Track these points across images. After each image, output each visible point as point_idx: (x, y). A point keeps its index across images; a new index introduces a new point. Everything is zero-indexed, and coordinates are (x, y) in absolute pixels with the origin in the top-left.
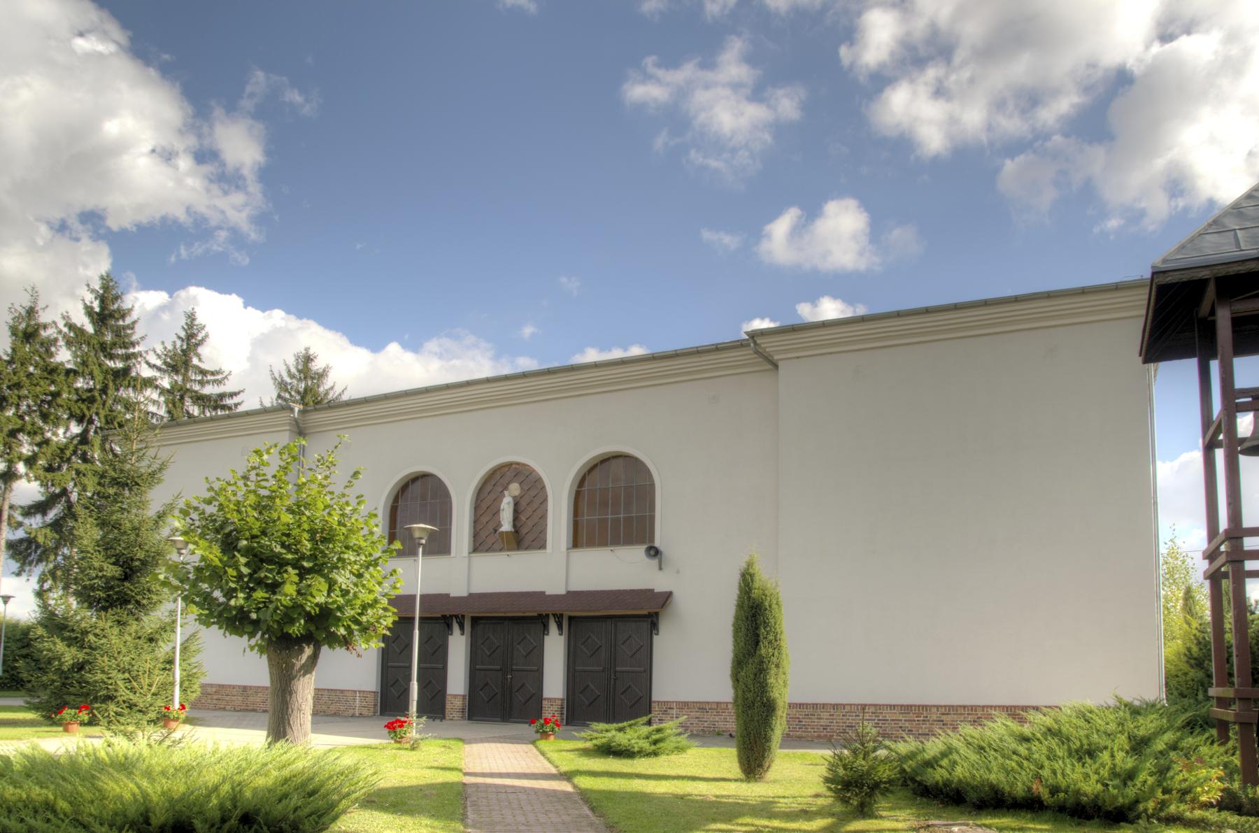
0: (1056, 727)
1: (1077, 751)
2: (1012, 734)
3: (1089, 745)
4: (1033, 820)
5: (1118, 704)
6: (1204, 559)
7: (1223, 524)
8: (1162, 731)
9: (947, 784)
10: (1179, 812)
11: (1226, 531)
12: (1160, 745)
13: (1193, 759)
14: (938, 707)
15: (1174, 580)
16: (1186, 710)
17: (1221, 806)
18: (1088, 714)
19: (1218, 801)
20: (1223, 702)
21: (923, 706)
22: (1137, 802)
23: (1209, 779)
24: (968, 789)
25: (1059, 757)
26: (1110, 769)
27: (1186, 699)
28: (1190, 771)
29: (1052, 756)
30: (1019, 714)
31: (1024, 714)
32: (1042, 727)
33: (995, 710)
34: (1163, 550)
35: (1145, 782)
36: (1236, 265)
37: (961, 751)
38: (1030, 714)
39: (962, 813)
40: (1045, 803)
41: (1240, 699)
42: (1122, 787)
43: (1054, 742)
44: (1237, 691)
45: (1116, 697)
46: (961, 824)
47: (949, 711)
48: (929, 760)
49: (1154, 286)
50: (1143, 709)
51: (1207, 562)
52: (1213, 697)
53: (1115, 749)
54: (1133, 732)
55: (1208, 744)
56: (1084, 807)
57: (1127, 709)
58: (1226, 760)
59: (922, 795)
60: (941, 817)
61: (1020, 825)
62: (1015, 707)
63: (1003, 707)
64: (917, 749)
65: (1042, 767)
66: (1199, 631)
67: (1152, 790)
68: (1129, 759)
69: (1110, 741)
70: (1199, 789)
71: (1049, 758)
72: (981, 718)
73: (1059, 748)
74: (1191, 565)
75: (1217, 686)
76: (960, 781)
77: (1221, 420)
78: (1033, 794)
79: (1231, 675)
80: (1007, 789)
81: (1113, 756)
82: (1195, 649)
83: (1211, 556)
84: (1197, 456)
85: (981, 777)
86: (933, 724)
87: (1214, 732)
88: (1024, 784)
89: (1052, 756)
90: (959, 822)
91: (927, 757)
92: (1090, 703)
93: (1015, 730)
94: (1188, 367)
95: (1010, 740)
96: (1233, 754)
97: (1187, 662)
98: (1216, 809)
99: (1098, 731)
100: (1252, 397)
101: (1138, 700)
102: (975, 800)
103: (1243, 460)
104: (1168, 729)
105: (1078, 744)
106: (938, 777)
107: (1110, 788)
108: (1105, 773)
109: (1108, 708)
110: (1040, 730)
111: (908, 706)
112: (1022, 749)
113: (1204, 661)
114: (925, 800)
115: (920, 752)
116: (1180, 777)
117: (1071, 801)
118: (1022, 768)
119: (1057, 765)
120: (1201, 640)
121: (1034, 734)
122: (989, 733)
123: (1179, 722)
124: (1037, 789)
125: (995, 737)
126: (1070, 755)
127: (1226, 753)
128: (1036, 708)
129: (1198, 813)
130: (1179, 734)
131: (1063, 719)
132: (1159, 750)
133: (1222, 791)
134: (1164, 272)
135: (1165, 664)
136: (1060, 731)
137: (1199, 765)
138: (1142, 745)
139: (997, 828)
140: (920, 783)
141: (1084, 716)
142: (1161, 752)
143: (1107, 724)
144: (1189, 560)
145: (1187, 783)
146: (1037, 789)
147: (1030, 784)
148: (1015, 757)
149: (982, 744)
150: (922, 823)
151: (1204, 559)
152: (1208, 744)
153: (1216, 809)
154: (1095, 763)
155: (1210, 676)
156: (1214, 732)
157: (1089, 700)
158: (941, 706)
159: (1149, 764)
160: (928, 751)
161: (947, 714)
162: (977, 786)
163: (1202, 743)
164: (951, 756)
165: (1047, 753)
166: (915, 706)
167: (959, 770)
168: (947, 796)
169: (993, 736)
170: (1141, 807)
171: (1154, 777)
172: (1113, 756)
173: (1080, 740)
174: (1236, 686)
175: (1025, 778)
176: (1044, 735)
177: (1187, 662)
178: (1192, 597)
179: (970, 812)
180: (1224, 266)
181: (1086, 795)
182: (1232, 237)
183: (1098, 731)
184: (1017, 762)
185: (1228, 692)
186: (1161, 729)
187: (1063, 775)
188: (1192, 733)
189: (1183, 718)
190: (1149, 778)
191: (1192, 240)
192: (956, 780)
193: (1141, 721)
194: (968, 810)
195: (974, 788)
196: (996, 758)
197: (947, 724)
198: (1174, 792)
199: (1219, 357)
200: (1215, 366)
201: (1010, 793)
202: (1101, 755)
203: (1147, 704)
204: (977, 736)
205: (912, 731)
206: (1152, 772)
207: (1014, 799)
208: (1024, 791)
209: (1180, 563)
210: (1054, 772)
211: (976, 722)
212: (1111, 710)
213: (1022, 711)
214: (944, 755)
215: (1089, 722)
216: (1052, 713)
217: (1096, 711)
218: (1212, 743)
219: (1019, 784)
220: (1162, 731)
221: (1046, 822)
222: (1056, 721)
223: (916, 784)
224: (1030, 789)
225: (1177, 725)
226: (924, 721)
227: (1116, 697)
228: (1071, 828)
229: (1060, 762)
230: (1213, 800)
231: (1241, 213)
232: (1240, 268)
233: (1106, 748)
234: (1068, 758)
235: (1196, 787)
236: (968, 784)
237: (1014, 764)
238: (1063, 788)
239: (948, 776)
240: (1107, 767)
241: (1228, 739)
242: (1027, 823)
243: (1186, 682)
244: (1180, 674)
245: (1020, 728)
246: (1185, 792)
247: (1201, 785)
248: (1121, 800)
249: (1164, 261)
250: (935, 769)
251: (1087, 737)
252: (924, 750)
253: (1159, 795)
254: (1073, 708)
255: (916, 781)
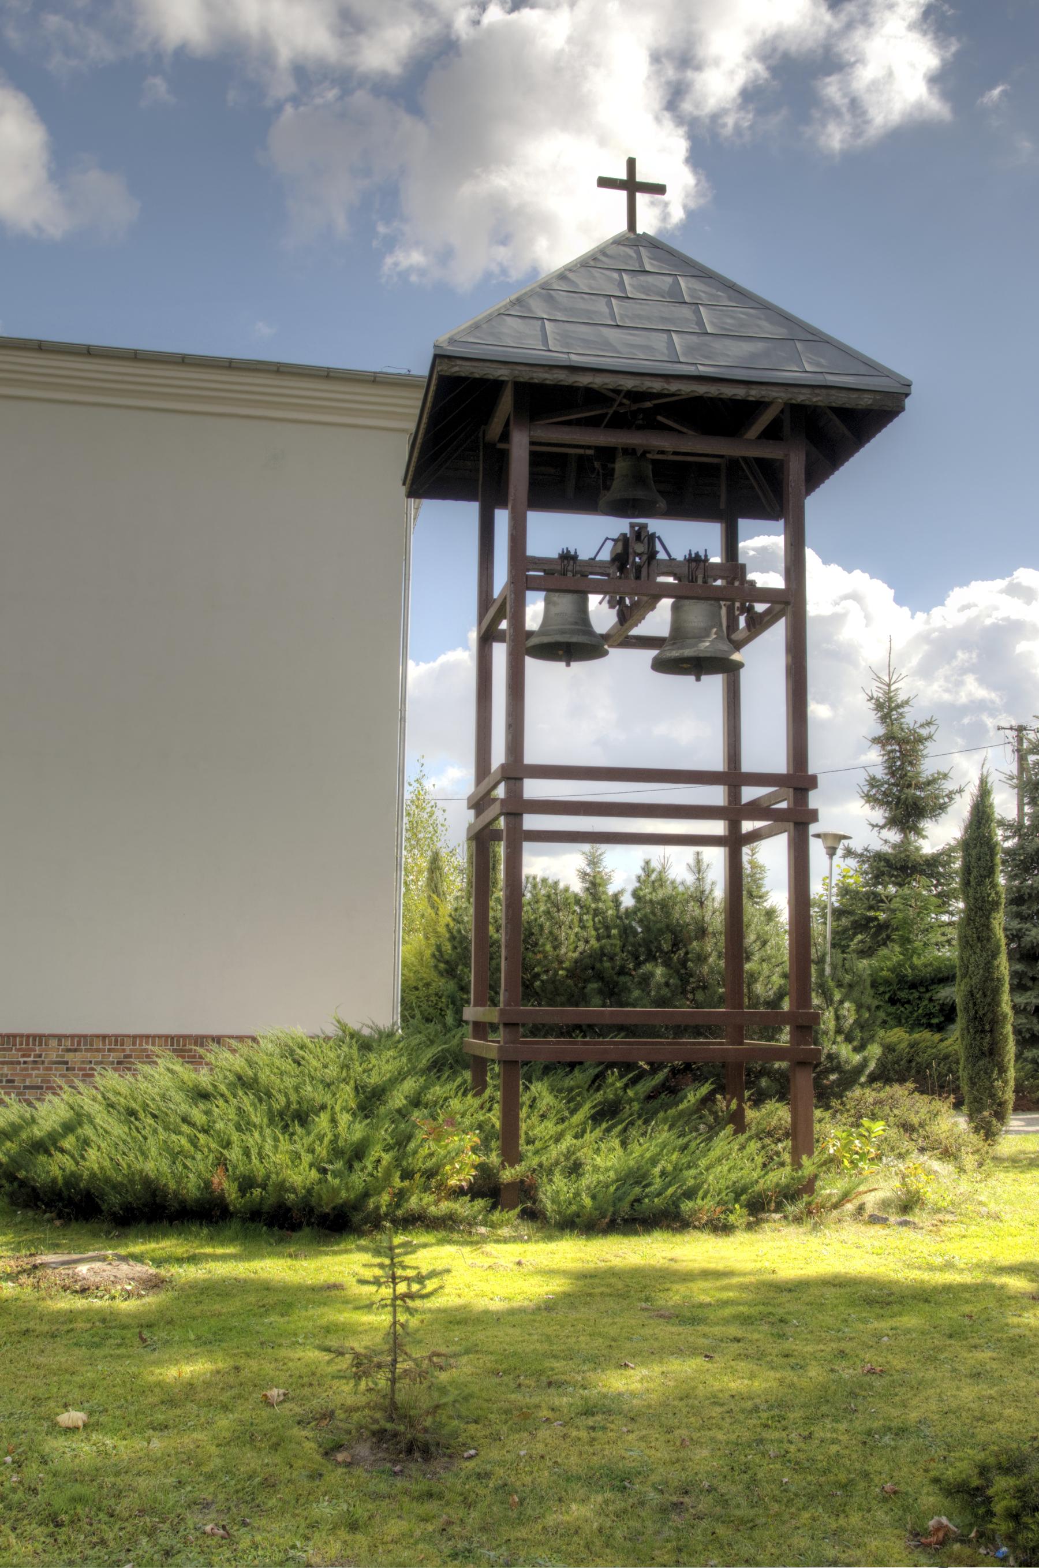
0: (250, 1073)
1: (281, 1114)
2: (182, 1087)
3: (299, 1103)
4: (211, 1239)
5: (340, 1033)
6: (469, 808)
7: (498, 756)
8: (399, 1077)
9: (72, 1180)
10: (422, 1207)
11: (503, 766)
12: (397, 1099)
13: (440, 1119)
14: (59, 1037)
15: (418, 841)
16: (432, 1042)
17: (474, 1191)
18: (298, 1051)
19: (471, 1186)
20: (481, 1029)
21: (34, 1036)
22: (366, 1195)
23: (460, 1152)
24: (107, 1189)
25: (255, 1126)
26: (331, 1142)
27: (431, 1025)
28: (438, 1140)
29: (244, 1125)
30: (190, 1050)
31: (200, 1050)
32: (228, 1073)
33: (153, 1044)
34: (408, 796)
35: (379, 1161)
36: (541, 370)
37: (98, 1121)
38: (210, 1051)
39: (95, 1235)
40: (231, 1208)
41: (506, 1025)
42: (346, 1172)
43: (247, 1101)
44: (502, 1013)
45: (339, 1022)
46: (92, 1259)
47: (79, 1044)
48: (42, 1139)
49: (435, 376)
50: (374, 1040)
51: (472, 812)
52: (467, 1022)
53: (337, 1108)
54: (362, 1080)
55: (460, 1094)
56: (289, 1210)
57: (354, 1041)
58: (482, 1118)
59: (26, 1206)
60: (58, 1246)
61: (192, 1251)
62: (185, 1037)
63: (167, 1037)
64: (22, 1117)
65: (228, 1145)
66: (454, 920)
67: (388, 1175)
68: (357, 1126)
69: (329, 1096)
70: (448, 1167)
71: (238, 1128)
72: (130, 1056)
73: (256, 1109)
74: (440, 820)
75: (475, 1006)
76: (93, 1175)
77: (505, 598)
78: (213, 1192)
79: (494, 988)
80: (172, 1185)
81: (333, 1121)
82: (447, 947)
83: (479, 803)
84: (466, 657)
85: (129, 1167)
86: (50, 1069)
87: (468, 1075)
88: (199, 1176)
89: (244, 1125)
90: (90, 1254)
91: (38, 1133)
92: (300, 1031)
93: (186, 1079)
94: (468, 512)
95: (178, 1097)
96: (490, 1110)
97: (436, 967)
98: (468, 1198)
99: (312, 1078)
100: (544, 571)
101: (368, 1027)
102: (116, 1209)
103: (532, 664)
104: (409, 1073)
105: (283, 1100)
106: (55, 1171)
107: (329, 1177)
108: (322, 1151)
109: (327, 1039)
110: (225, 1078)
111: (8, 1036)
112: (197, 1115)
113: (457, 965)
114: (30, 1214)
115: (28, 1124)
116: (424, 1151)
117: (272, 1200)
118: (195, 1147)
119: (250, 1140)
120: (455, 933)
121: (215, 1086)
122: (143, 1085)
123: (424, 1061)
124: (220, 1184)
125: (154, 1091)
126: (271, 1122)
127: (482, 1108)
128: (218, 1040)
129: (446, 1206)
130: (422, 1080)
131: (261, 1059)
132: (397, 1107)
133: (475, 1167)
134: (449, 357)
135: (403, 969)
136: (256, 1080)
137: (450, 1129)
138: (374, 1099)
139: (153, 1260)
140: (23, 1184)
141: (292, 1052)
142: (399, 1111)
143: (325, 1066)
144: (438, 813)
145: (434, 1160)
146: (220, 1184)
147: (208, 1175)
148: (185, 1128)
149: (134, 1105)
150: (25, 1263)
151: (469, 808)
152: (460, 1094)
153: (468, 1198)
154: (309, 1134)
155: (464, 989)
156: (468, 1075)
157: (299, 1027)
158: (66, 1036)
159: (384, 1133)
160: (40, 1121)
161: (75, 1050)
162: (121, 1184)
163: (452, 1093)
164: (79, 1131)
165: (236, 1118)
166: (21, 1036)
167: (92, 1154)
168: (70, 1202)
169: (150, 1090)
170: (371, 1204)
171: (391, 1154)
172: (333, 1121)
173: (286, 1095)
174: (502, 1005)
175: (201, 1167)
176: (231, 1086)
177: (436, 967)
178: (439, 868)
179: (108, 1233)
180: (527, 369)
181: (294, 1191)
182: (539, 328)
183: (312, 1078)
184: (188, 1136)
185: (490, 1014)
186: (399, 1074)
187: (261, 1157)
188: (439, 1078)
189: (429, 1055)
190: (383, 1155)
191: (489, 319)
192: (86, 1174)
193: (374, 1061)
194: (105, 1227)
195: (116, 1187)
196: (155, 1131)
197: (74, 1069)
198: (417, 1176)
199: (510, 506)
200: (502, 518)
201: (176, 1193)
202: (317, 1119)
203: (380, 1033)
204: (124, 1090)
205: (12, 1081)
206: (388, 1144)
207: (183, 1203)
208: (199, 1188)
209: (426, 816)
210: (247, 1152)
211: (123, 1065)
212: (331, 1043)
213: (196, 1044)
214: (68, 1128)
215: (299, 1064)
216: (244, 1049)
217: (311, 1046)
218: (465, 1094)
219: (191, 1176)
220: (399, 1077)
221: (231, 1241)
222: (250, 1063)
223: (16, 1184)
224: (208, 1184)
225: (421, 1066)
226: (35, 1062)
227: (339, 1022)
228: (269, 1249)
229: (256, 1134)
230: (464, 1183)
231: (551, 297)
232: (547, 376)
233: (323, 1107)
234: (268, 1126)
235: (444, 1165)
236: (107, 1180)
237: (184, 1141)
238: (260, 1180)
239: (74, 1168)
240: (326, 1140)
241: (484, 1086)
242: (202, 1246)
243: (428, 996)
244: (420, 985)
245: (193, 1076)
246: (430, 1174)
247: (452, 1162)
248: (344, 1194)
249: (452, 341)
250: (51, 1155)
251: (297, 1089)
252: (33, 1120)
253: (397, 1183)
254: (277, 1042)
255: (16, 1178)
